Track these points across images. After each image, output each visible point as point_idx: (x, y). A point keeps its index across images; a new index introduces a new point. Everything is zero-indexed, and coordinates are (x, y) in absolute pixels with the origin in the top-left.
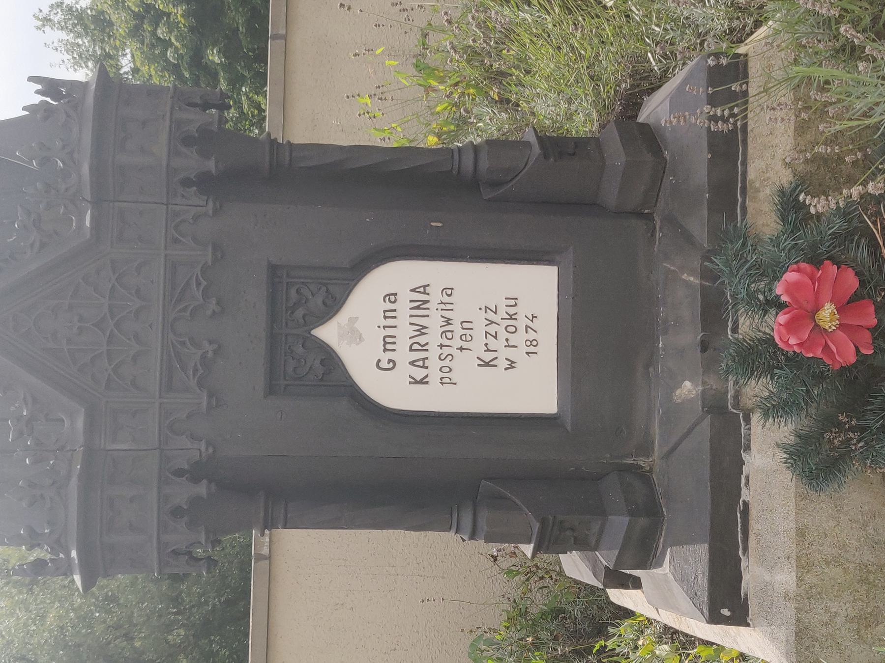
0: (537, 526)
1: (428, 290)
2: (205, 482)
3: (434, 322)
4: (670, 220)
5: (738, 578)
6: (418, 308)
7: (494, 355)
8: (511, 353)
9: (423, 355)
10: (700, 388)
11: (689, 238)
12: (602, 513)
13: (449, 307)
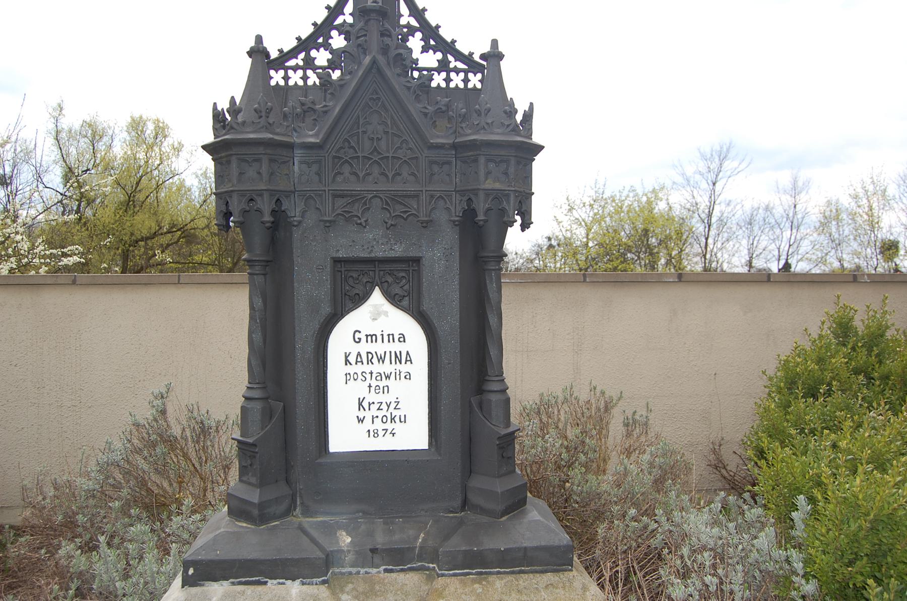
0: (250, 440)
1: (409, 363)
2: (272, 219)
3: (387, 368)
4: (461, 522)
5: (215, 580)
6: (396, 356)
7: (367, 408)
8: (368, 420)
9: (365, 361)
10: (345, 549)
11: (447, 537)
12: (262, 484)
13: (398, 377)
